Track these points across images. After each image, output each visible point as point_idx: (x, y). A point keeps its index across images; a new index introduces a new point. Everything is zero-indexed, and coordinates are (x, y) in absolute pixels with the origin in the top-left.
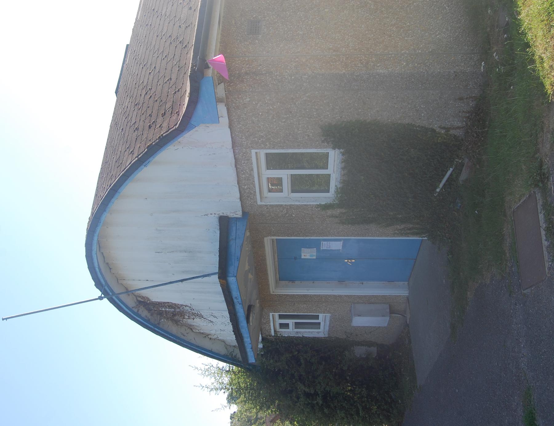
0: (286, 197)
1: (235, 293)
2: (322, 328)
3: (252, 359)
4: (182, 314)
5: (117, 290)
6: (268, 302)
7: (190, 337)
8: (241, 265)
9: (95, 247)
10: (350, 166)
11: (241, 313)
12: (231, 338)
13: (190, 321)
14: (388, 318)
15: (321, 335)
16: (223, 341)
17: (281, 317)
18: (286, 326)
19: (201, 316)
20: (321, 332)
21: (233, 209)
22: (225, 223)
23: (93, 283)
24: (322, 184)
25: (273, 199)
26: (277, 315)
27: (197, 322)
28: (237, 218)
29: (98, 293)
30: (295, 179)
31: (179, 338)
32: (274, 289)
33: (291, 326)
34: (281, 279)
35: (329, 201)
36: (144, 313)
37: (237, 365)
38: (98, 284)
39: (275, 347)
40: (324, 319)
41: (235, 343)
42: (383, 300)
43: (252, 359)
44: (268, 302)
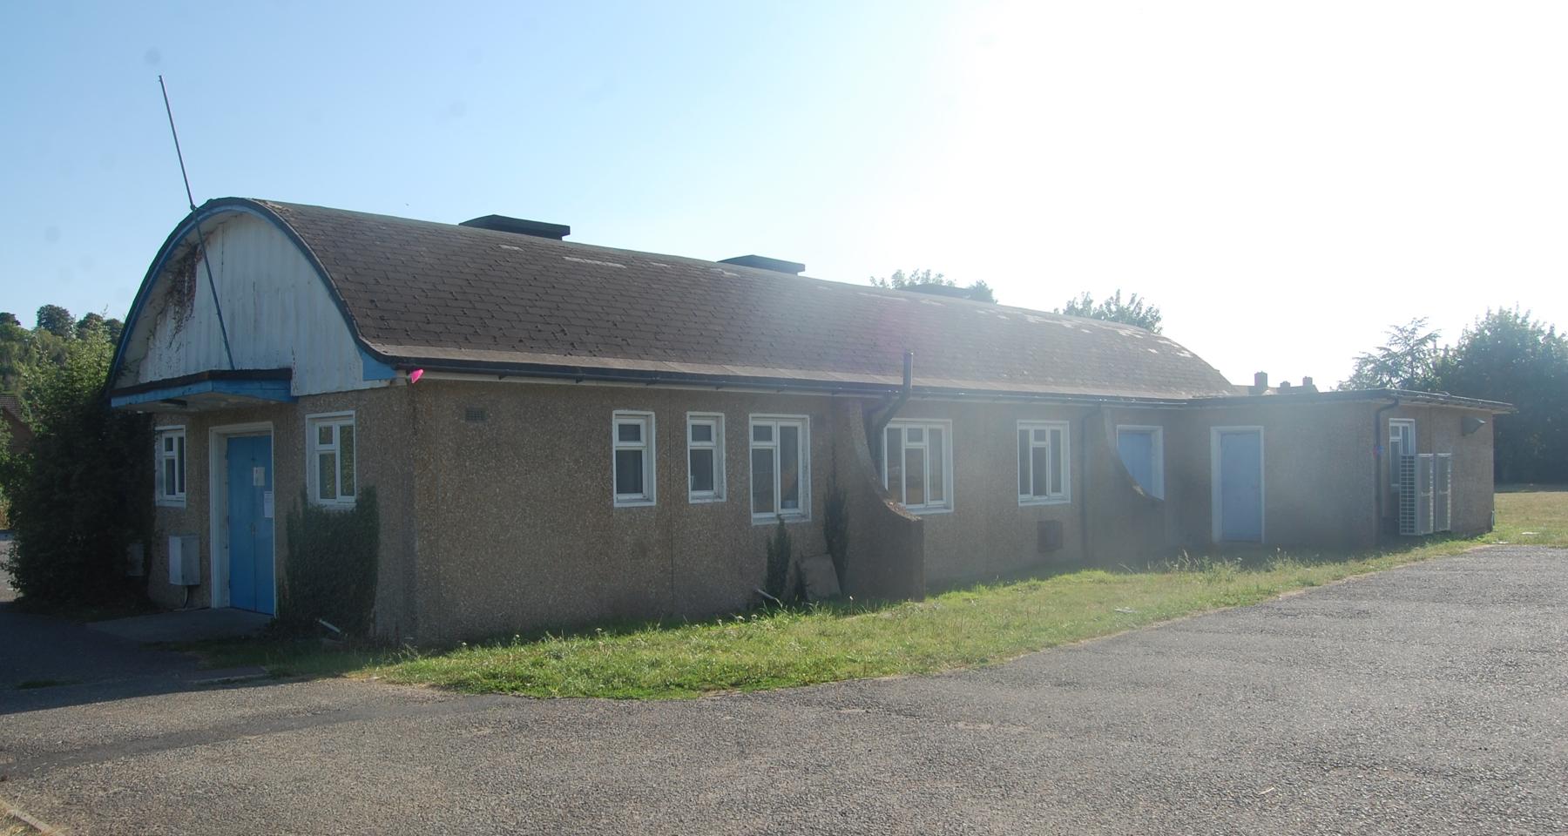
0: (314, 449)
1: (195, 389)
3: (116, 403)
4: (181, 303)
5: (205, 227)
6: (201, 421)
7: (148, 312)
8: (231, 396)
10: (345, 517)
11: (175, 393)
12: (151, 374)
13: (171, 314)
14: (180, 583)
15: (158, 497)
16: (145, 356)
17: (181, 440)
19: (178, 329)
20: (162, 497)
21: (303, 385)
22: (283, 376)
23: (214, 198)
25: (312, 432)
26: (183, 434)
27: (171, 324)
28: (289, 390)
29: (199, 202)
30: (769, 453)
31: (146, 296)
32: (215, 431)
33: (326, 448)
34: (230, 441)
35: (310, 498)
36: (180, 253)
37: (108, 378)
38: (212, 204)
39: (139, 430)
40: (179, 500)
42: (206, 577)
43: (116, 403)
44: (201, 421)
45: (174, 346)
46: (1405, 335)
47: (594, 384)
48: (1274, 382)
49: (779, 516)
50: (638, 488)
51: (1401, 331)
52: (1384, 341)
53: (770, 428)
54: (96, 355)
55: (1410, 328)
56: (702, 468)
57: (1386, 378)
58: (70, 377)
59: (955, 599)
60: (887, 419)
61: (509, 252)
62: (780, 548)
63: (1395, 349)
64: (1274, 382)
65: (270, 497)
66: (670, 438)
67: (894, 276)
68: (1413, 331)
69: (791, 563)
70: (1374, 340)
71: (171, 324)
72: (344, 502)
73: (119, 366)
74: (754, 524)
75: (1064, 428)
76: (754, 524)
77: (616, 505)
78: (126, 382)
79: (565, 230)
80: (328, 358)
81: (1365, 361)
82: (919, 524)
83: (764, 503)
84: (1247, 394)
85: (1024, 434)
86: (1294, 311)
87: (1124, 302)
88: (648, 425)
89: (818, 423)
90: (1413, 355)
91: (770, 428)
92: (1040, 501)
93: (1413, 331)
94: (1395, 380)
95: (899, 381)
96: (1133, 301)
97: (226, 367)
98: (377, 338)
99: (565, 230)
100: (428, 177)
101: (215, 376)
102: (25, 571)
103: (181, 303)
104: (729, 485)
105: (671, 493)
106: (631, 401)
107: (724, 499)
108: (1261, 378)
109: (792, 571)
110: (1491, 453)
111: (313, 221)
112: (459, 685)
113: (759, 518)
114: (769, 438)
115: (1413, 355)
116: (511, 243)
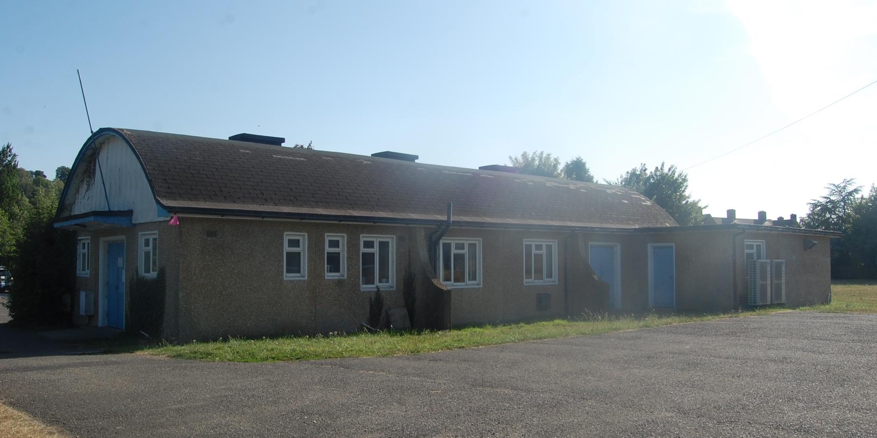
0: (142, 249)
2: (83, 272)
3: (56, 225)
4: (89, 177)
5: (97, 142)
9: (112, 133)
12: (78, 210)
13: (85, 182)
15: (78, 272)
17: (155, 240)
18: (84, 248)
21: (138, 219)
22: (129, 213)
24: (147, 270)
25: (141, 241)
27: (85, 187)
29: (94, 131)
30: (541, 255)
32: (103, 240)
33: (147, 248)
35: (140, 272)
36: (89, 152)
38: (101, 130)
39: (69, 239)
41: (73, 214)
42: (97, 311)
43: (56, 225)
45: (86, 198)
46: (839, 189)
47: (272, 219)
48: (772, 216)
49: (377, 287)
50: (337, 270)
51: (837, 187)
52: (826, 193)
53: (373, 242)
54: (49, 202)
55: (842, 185)
56: (334, 262)
57: (828, 215)
58: (38, 212)
59: (489, 333)
60: (440, 238)
61: (243, 154)
62: (377, 302)
63: (833, 198)
64: (739, 215)
65: (124, 272)
66: (316, 247)
67: (523, 155)
68: (844, 188)
69: (384, 310)
70: (820, 193)
71: (85, 187)
72: (153, 275)
73: (63, 205)
74: (362, 290)
75: (555, 245)
76: (362, 290)
77: (285, 279)
78: (65, 214)
79: (283, 140)
80: (145, 206)
81: (815, 206)
82: (449, 292)
83: (369, 280)
84: (719, 223)
85: (529, 247)
86: (756, 177)
87: (666, 170)
88: (304, 239)
89: (400, 240)
90: (845, 202)
91: (373, 242)
92: (539, 282)
93: (844, 188)
94: (833, 216)
95: (445, 218)
96: (670, 169)
97: (107, 209)
98: (164, 197)
99: (283, 140)
100: (209, 116)
101: (95, 214)
102: (13, 307)
103: (89, 177)
104: (348, 270)
105: (316, 274)
106: (294, 227)
107: (346, 277)
108: (762, 215)
109: (383, 314)
110: (828, 260)
111: (144, 141)
112: (180, 356)
113: (365, 288)
114: (373, 247)
115: (845, 202)
116: (246, 149)
